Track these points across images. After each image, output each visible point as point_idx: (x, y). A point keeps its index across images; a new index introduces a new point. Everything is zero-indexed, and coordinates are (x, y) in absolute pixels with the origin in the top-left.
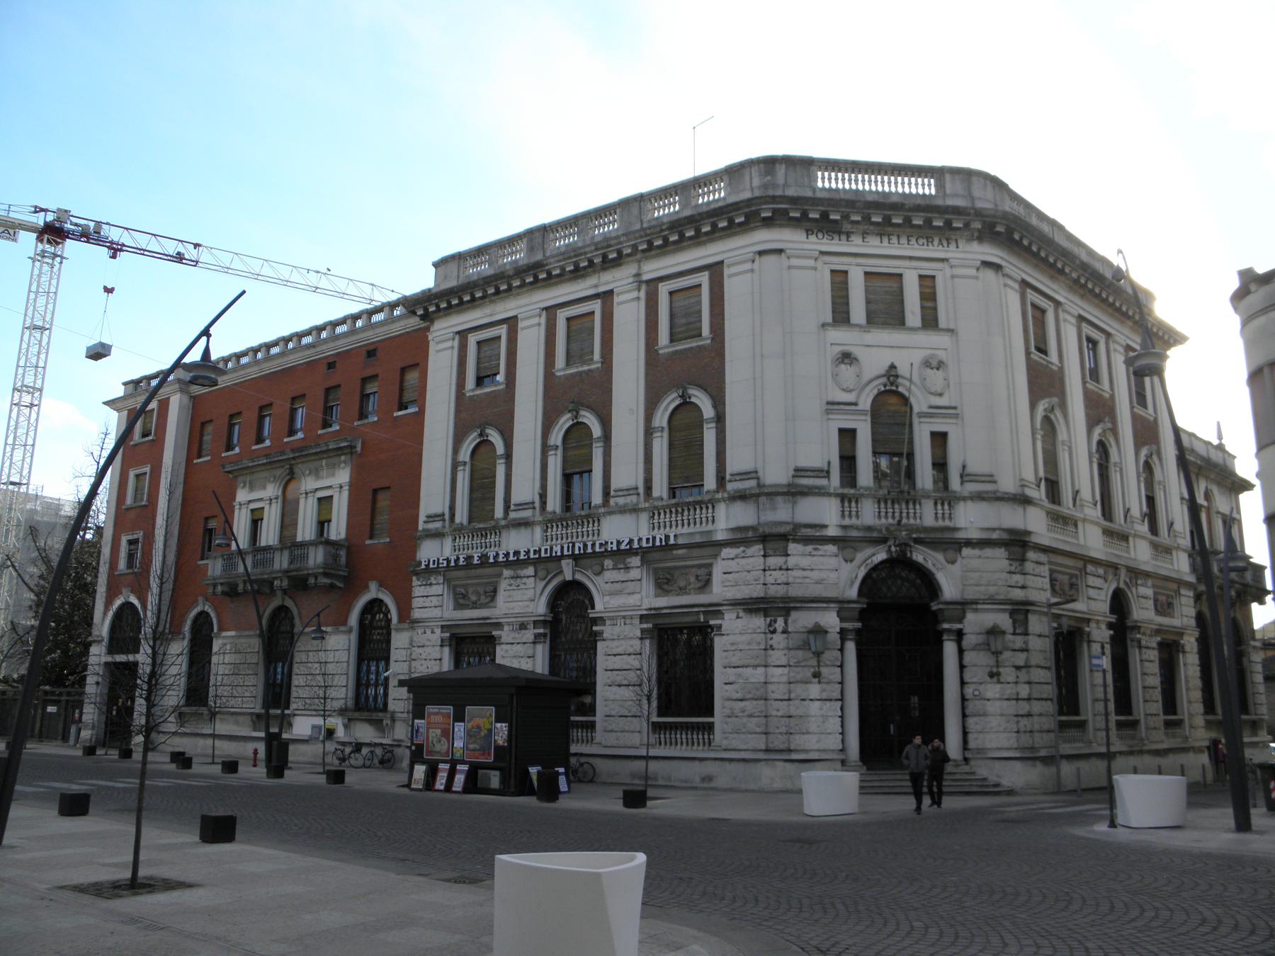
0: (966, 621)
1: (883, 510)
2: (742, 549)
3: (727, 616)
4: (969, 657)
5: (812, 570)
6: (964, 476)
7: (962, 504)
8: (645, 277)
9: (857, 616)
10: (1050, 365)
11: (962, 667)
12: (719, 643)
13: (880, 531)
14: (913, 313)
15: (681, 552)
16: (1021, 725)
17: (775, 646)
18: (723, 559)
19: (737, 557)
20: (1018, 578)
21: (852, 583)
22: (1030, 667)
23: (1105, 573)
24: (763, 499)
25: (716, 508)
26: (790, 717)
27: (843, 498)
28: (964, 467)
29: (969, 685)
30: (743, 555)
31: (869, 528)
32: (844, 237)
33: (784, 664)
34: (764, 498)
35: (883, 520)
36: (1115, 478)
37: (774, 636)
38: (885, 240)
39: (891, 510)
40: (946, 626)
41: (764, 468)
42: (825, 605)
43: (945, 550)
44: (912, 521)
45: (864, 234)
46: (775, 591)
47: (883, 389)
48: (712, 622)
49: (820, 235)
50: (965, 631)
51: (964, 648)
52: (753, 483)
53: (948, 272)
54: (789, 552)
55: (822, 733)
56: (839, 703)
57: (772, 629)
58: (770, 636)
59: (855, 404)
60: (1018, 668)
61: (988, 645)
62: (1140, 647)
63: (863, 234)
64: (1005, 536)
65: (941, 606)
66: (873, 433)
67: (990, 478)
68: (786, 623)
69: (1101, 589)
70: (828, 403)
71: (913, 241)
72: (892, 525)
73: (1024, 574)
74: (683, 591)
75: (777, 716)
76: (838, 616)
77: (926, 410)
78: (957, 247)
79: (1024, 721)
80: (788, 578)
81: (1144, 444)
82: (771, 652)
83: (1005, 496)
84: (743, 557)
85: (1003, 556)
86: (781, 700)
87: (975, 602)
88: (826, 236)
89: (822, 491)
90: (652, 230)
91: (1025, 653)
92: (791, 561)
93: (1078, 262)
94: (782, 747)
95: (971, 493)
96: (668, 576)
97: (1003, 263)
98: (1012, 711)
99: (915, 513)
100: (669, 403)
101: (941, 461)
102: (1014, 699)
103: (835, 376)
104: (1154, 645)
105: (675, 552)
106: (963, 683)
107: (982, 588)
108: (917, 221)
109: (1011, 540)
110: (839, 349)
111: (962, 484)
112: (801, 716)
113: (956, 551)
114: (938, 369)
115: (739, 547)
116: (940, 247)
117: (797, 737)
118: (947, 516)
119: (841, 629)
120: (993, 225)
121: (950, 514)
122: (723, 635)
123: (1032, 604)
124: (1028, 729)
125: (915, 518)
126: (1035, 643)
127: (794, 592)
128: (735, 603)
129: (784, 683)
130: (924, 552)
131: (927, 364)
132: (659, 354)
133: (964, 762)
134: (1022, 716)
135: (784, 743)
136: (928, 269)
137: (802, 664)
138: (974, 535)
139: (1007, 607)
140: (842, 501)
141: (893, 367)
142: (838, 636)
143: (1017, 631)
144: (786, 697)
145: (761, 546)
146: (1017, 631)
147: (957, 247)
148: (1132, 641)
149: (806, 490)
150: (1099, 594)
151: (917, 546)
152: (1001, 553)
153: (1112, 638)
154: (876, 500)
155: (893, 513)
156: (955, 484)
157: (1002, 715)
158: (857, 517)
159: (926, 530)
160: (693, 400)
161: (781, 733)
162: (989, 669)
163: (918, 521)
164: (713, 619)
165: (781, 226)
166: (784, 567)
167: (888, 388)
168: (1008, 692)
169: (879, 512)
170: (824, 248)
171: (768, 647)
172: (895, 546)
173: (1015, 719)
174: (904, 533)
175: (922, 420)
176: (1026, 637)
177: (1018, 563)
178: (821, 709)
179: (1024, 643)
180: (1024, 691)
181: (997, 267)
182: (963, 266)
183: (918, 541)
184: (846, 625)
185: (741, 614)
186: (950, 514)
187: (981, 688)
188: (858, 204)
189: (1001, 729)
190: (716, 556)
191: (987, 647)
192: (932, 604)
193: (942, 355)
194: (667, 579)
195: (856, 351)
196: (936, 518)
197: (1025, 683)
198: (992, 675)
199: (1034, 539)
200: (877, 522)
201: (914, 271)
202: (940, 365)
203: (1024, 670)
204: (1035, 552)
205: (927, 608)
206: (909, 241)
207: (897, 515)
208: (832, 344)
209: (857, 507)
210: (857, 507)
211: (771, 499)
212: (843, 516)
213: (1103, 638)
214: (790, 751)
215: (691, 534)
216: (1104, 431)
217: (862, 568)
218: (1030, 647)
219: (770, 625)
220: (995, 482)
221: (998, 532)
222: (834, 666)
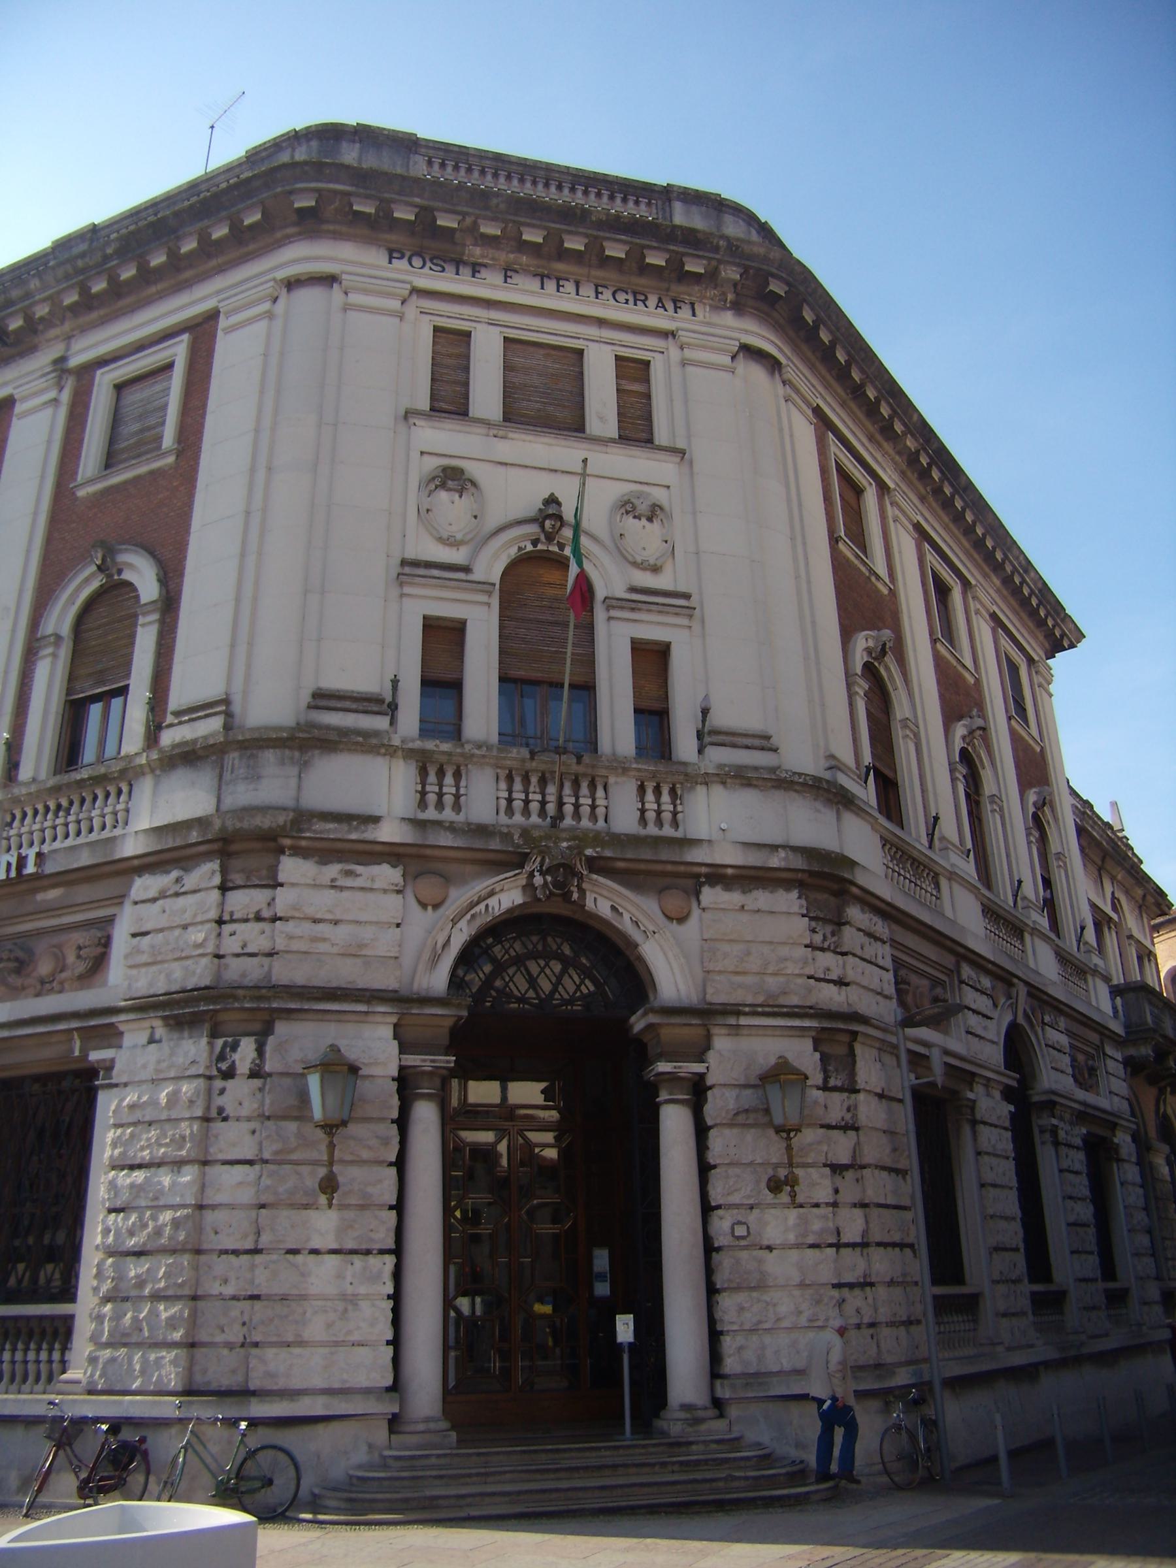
0: (711, 1056)
1: (519, 795)
2: (175, 874)
3: (128, 1040)
4: (718, 1143)
5: (336, 922)
6: (706, 736)
7: (701, 790)
8: (74, 362)
9: (446, 1042)
10: (873, 579)
11: (704, 1169)
12: (108, 1105)
13: (507, 837)
14: (601, 419)
15: (53, 894)
16: (849, 1308)
17: (230, 1110)
18: (136, 903)
19: (162, 895)
20: (827, 960)
21: (435, 959)
22: (863, 1167)
23: (993, 988)
24: (233, 758)
25: (135, 788)
26: (255, 1297)
27: (423, 762)
28: (705, 712)
29: (720, 1212)
30: (176, 888)
31: (482, 830)
32: (466, 271)
33: (249, 1157)
34: (236, 754)
35: (518, 818)
36: (993, 823)
37: (230, 1084)
38: (551, 286)
39: (539, 797)
40: (663, 1067)
41: (245, 693)
42: (362, 1008)
43: (661, 891)
44: (585, 823)
45: (508, 272)
46: (238, 970)
47: (530, 548)
48: (95, 1056)
49: (417, 262)
50: (710, 1081)
51: (710, 1122)
52: (214, 725)
53: (674, 353)
54: (281, 878)
55: (336, 1344)
56: (390, 1260)
57: (224, 1066)
58: (218, 1084)
59: (466, 569)
60: (837, 1169)
61: (767, 1111)
62: (1057, 1144)
63: (506, 270)
64: (798, 862)
65: (653, 1019)
66: (503, 636)
67: (763, 742)
68: (260, 1051)
69: (991, 1018)
70: (404, 563)
71: (607, 294)
72: (535, 826)
73: (844, 954)
74: (45, 986)
75: (221, 1297)
76: (396, 1036)
77: (621, 593)
78: (694, 315)
79: (855, 1299)
80: (273, 938)
81: (1031, 786)
82: (219, 1126)
83: (796, 778)
84: (177, 895)
85: (795, 909)
86: (236, 1252)
87: (735, 1010)
88: (429, 264)
89: (374, 741)
90: (87, 259)
91: (852, 1133)
92: (284, 899)
93: (915, 418)
94: (226, 1382)
95: (721, 766)
96: (20, 954)
97: (783, 360)
98: (826, 1275)
99: (593, 807)
100: (79, 589)
101: (656, 706)
102: (830, 1245)
103: (425, 513)
104: (1078, 1141)
105: (40, 897)
106: (707, 1209)
107: (749, 980)
108: (616, 251)
109: (811, 873)
110: (432, 463)
111: (700, 751)
112: (284, 1298)
113: (686, 892)
114: (650, 519)
115: (168, 872)
116: (660, 310)
117: (270, 1353)
118: (667, 816)
119: (402, 1068)
120: (763, 277)
121: (675, 814)
122: (116, 1085)
123: (864, 1020)
124: (866, 1320)
125: (593, 817)
126: (870, 1111)
127: (285, 972)
128: (144, 1006)
129: (243, 1207)
130: (611, 890)
131: (627, 507)
132: (76, 499)
133: (712, 1412)
134: (851, 1286)
135: (234, 1372)
136: (637, 347)
137: (294, 1157)
138: (728, 856)
139: (807, 1023)
140: (423, 772)
141: (552, 501)
142: (395, 1085)
143: (832, 1082)
144: (249, 1245)
145: (214, 865)
146: (832, 1082)
147: (694, 315)
148: (1042, 1132)
149: (333, 736)
150: (985, 1028)
151: (595, 876)
152: (789, 900)
153: (1013, 1116)
154: (503, 773)
155: (543, 803)
156: (685, 745)
157: (802, 1285)
158: (457, 807)
159: (618, 840)
160: (127, 576)
161: (230, 1346)
162: (770, 1172)
163: (601, 823)
164: (96, 1048)
165: (337, 236)
166: (266, 914)
167: (540, 547)
168: (817, 1226)
169: (510, 800)
170: (423, 283)
171: (214, 1113)
172: (542, 873)
173: (835, 1293)
174: (565, 844)
175: (613, 613)
176: (853, 1096)
177: (829, 929)
178: (340, 1276)
179: (848, 1110)
180: (853, 1226)
181: (773, 365)
182: (704, 347)
183: (597, 866)
184: (412, 1060)
185: (160, 1032)
186: (675, 814)
187: (753, 1217)
188: (495, 201)
189: (803, 1321)
190: (119, 899)
191: (766, 1120)
192: (633, 1019)
193: (659, 495)
194: (17, 959)
195: (471, 468)
196: (643, 821)
197: (855, 1205)
198: (775, 1186)
199: (861, 879)
200: (503, 819)
201: (610, 347)
202: (654, 513)
203: (850, 1175)
204: (863, 911)
205: (623, 1026)
206: (597, 293)
207: (551, 808)
208: (422, 453)
209: (458, 788)
210: (458, 788)
211: (252, 756)
212: (422, 804)
213: (999, 1118)
214: (245, 1393)
215: (72, 848)
216: (971, 732)
217: (463, 924)
218: (863, 1120)
219: (221, 1057)
220: (775, 750)
221: (782, 853)
222: (379, 1163)
